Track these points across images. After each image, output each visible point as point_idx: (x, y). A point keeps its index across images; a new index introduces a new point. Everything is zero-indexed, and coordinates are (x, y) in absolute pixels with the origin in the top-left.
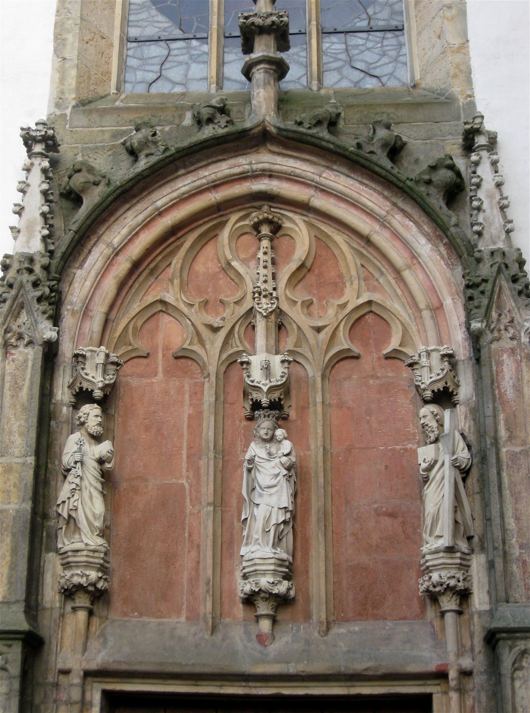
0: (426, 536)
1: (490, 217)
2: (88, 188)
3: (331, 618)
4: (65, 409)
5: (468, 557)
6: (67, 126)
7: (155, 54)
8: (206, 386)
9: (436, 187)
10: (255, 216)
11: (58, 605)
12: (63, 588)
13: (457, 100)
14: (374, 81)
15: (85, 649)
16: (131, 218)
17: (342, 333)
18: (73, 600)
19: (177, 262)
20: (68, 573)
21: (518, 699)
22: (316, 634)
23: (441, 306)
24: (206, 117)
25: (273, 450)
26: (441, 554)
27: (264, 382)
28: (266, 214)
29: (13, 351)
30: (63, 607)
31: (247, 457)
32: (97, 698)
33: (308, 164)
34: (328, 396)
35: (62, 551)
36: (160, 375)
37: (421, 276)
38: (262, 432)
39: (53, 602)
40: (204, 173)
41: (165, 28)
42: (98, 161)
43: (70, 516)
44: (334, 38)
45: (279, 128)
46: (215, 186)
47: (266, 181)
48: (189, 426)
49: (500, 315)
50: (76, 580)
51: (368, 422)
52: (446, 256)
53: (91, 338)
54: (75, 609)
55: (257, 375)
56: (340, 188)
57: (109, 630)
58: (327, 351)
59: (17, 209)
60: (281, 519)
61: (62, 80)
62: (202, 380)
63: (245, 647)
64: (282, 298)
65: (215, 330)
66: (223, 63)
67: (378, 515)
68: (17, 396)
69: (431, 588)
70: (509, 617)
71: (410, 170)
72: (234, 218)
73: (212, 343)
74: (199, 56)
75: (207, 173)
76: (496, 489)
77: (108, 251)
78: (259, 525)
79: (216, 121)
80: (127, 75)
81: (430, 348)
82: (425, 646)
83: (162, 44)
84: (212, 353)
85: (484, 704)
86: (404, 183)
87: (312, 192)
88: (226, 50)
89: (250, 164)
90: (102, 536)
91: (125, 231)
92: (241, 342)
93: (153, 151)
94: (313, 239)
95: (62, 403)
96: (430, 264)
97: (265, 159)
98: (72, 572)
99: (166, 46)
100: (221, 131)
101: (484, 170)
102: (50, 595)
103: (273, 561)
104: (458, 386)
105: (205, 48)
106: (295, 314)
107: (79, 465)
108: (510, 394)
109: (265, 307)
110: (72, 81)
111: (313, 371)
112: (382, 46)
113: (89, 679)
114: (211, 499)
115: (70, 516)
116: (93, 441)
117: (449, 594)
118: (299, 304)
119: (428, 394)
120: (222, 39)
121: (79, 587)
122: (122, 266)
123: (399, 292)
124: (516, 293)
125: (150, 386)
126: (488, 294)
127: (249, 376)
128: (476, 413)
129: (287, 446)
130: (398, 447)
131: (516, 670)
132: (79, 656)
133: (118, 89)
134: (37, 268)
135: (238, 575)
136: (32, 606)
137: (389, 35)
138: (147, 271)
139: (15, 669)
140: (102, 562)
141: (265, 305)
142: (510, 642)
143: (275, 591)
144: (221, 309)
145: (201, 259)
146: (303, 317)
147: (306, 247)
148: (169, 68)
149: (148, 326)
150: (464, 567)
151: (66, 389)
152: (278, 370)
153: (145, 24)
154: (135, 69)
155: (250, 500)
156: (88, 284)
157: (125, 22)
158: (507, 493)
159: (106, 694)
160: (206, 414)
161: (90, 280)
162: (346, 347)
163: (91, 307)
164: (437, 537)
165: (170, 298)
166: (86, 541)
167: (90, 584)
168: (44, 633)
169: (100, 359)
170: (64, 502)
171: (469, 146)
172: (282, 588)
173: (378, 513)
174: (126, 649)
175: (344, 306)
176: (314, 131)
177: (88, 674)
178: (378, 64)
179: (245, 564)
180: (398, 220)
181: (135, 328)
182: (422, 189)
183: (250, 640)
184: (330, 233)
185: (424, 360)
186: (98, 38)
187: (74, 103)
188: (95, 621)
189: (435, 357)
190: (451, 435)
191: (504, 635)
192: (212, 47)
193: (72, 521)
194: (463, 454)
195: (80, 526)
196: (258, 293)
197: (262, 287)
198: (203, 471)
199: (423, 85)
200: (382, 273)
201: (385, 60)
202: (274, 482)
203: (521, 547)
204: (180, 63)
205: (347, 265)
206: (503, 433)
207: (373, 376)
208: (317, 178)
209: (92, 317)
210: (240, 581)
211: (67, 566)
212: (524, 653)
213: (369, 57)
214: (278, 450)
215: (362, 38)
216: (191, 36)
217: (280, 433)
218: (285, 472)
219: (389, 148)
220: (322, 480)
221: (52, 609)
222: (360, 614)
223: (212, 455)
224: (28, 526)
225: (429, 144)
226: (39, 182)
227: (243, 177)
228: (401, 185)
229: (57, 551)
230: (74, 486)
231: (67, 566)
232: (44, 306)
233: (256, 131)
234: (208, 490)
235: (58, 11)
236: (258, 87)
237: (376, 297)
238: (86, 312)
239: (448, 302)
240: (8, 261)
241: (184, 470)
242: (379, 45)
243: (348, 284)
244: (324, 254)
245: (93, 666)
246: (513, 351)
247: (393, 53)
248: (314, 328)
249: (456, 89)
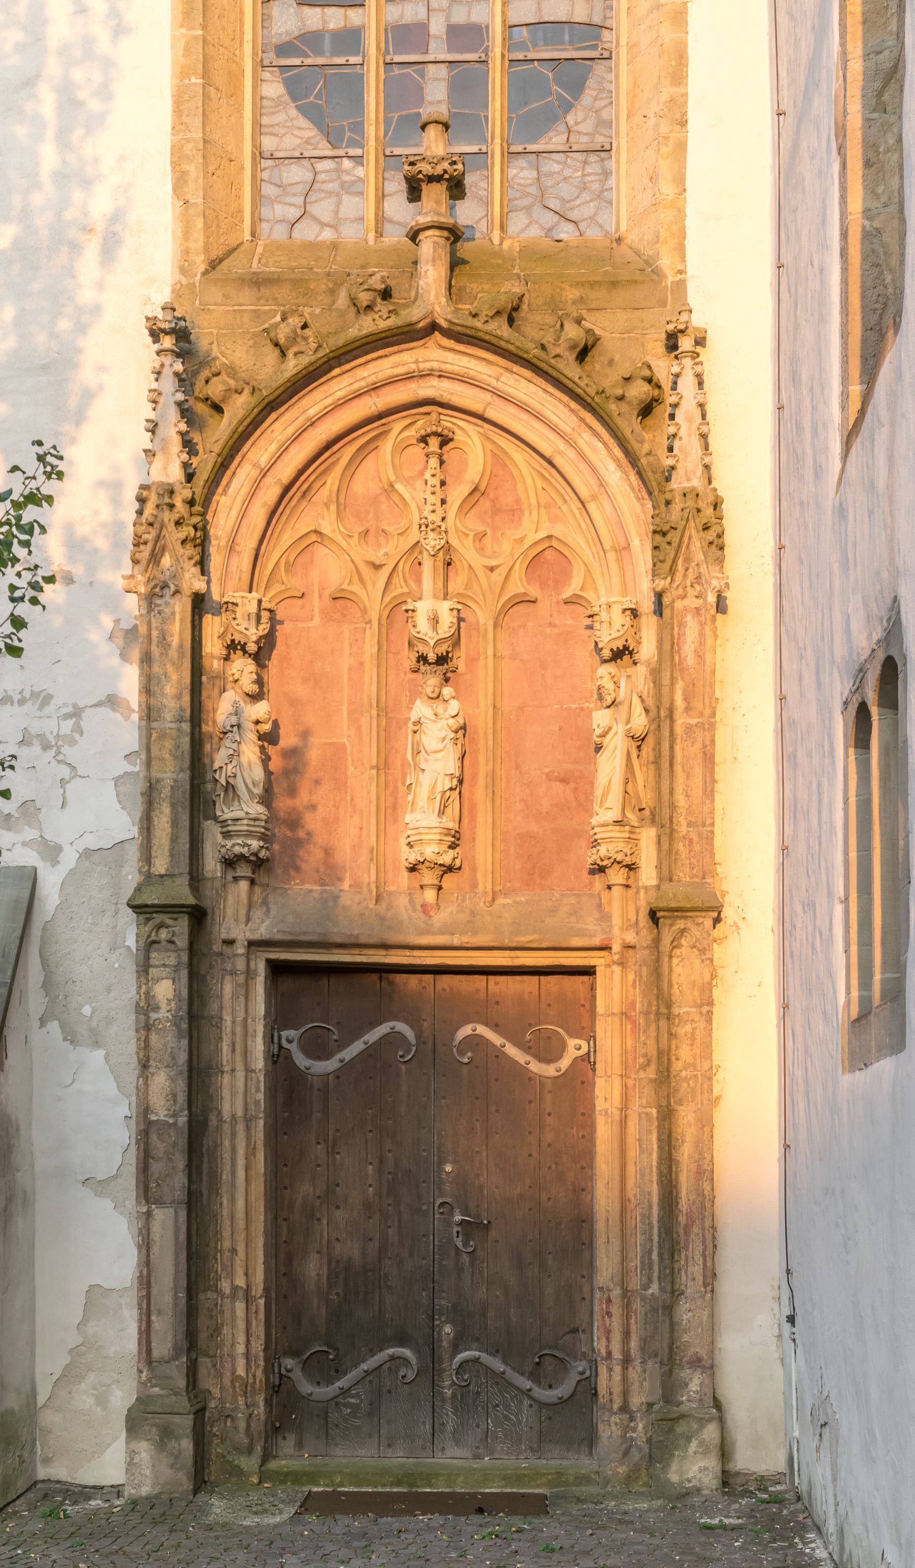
0: (596, 807)
1: (688, 443)
2: (229, 397)
3: (497, 888)
4: (216, 663)
5: (638, 830)
6: (197, 302)
7: (296, 179)
8: (368, 632)
9: (630, 403)
10: (422, 425)
11: (219, 874)
12: (223, 857)
13: (665, 276)
14: (570, 227)
15: (248, 920)
16: (280, 427)
17: (518, 573)
18: (234, 869)
19: (332, 484)
20: (229, 843)
21: (674, 976)
22: (482, 904)
23: (628, 547)
24: (365, 304)
25: (440, 710)
26: (610, 828)
27: (430, 634)
28: (436, 425)
29: (158, 602)
30: (224, 877)
31: (414, 716)
32: (261, 967)
33: (484, 363)
34: (499, 646)
35: (221, 819)
36: (317, 619)
37: (608, 508)
38: (429, 690)
39: (215, 871)
40: (362, 373)
41: (309, 138)
42: (237, 354)
43: (228, 782)
44: (522, 162)
45: (450, 322)
46: (375, 388)
47: (435, 382)
48: (350, 679)
49: (687, 569)
50: (237, 850)
51: (543, 676)
52: (636, 488)
53: (240, 579)
54: (236, 879)
55: (423, 626)
56: (521, 396)
57: (271, 898)
58: (500, 595)
59: (151, 426)
60: (448, 786)
61: (186, 234)
62: (363, 625)
63: (410, 917)
64: (452, 531)
65: (377, 567)
66: (383, 196)
67: (550, 780)
68: (167, 654)
69: (599, 862)
70: (674, 895)
71: (602, 376)
72: (398, 427)
73: (374, 584)
74: (353, 183)
75: (366, 374)
76: (667, 764)
77: (255, 473)
78: (424, 792)
79: (376, 309)
80: (263, 209)
81: (611, 600)
82: (591, 919)
83: (305, 162)
84: (373, 597)
85: (645, 979)
86: (593, 399)
87: (487, 396)
88: (387, 175)
89: (417, 362)
90: (262, 803)
91: (273, 448)
92: (406, 581)
93: (303, 349)
94: (489, 454)
95: (213, 657)
96: (618, 496)
97: (433, 354)
98: (233, 842)
99: (310, 166)
100: (383, 325)
101: (687, 384)
102: (212, 866)
103: (438, 830)
104: (639, 643)
105: (360, 172)
106: (466, 551)
107: (235, 729)
108: (691, 660)
109: (433, 543)
110: (198, 239)
111: (482, 616)
112: (584, 175)
113: (253, 948)
114: (374, 762)
115: (228, 782)
116: (248, 699)
117: (616, 866)
118: (471, 537)
119: (607, 654)
120: (382, 158)
121: (241, 857)
122: (270, 494)
123: (584, 526)
124: (705, 544)
125: (304, 629)
126: (675, 545)
127: (414, 626)
128: (655, 674)
129: (454, 706)
130: (574, 706)
131: (674, 948)
132: (242, 926)
133: (253, 235)
134: (178, 502)
135: (403, 841)
136: (196, 879)
137: (593, 158)
138: (299, 494)
139: (182, 942)
140: (263, 830)
141: (432, 541)
142: (669, 922)
143: (440, 861)
144: (382, 540)
145: (360, 477)
146: (473, 552)
147: (480, 468)
148: (316, 201)
149: (301, 560)
150: (632, 840)
151: (216, 640)
152: (447, 620)
153: (283, 131)
154: (272, 201)
155: (415, 764)
156: (234, 513)
157: (258, 128)
158: (678, 768)
159: (269, 962)
160: (367, 666)
161: (236, 509)
162: (522, 590)
163: (238, 540)
164: (606, 812)
165: (326, 528)
166: (246, 809)
167: (252, 854)
168: (207, 904)
169: (253, 608)
170: (221, 768)
171: (672, 344)
172: (447, 859)
173: (550, 777)
174: (290, 919)
175: (521, 540)
176: (492, 326)
177: (251, 944)
178: (577, 202)
179: (409, 832)
180: (585, 439)
181: (287, 563)
182: (613, 407)
183: (415, 910)
184: (508, 450)
185: (604, 615)
186: (225, 162)
187: (202, 268)
188: (258, 889)
189: (617, 609)
190: (628, 701)
191: (666, 914)
192: (368, 172)
193: (231, 789)
194: (640, 722)
195: (239, 793)
196: (424, 525)
197: (430, 519)
198: (365, 730)
199: (629, 241)
200: (565, 501)
201: (586, 196)
202: (440, 746)
203: (689, 825)
204: (330, 193)
205: (526, 489)
206: (679, 703)
207: (551, 625)
208: (494, 383)
209: (239, 553)
210: (405, 849)
211: (227, 835)
212: (683, 931)
213: (566, 190)
214: (445, 710)
215: (558, 162)
216: (341, 152)
217: (447, 691)
218: (452, 735)
219: (578, 350)
220: (491, 743)
221: (213, 879)
222: (527, 885)
223: (374, 713)
224: (188, 796)
225: (628, 341)
226: (173, 390)
227: (409, 377)
228: (589, 400)
229: (215, 818)
230: (231, 752)
231: (227, 835)
232: (190, 550)
233: (421, 324)
234: (371, 754)
235: (173, 128)
236: (427, 264)
237: (558, 531)
238: (232, 547)
239: (636, 542)
240: (145, 493)
241: (345, 728)
242: (579, 173)
243: (526, 513)
244: (501, 473)
245: (256, 936)
246: (698, 610)
247: (596, 186)
248: (486, 567)
249: (666, 262)
